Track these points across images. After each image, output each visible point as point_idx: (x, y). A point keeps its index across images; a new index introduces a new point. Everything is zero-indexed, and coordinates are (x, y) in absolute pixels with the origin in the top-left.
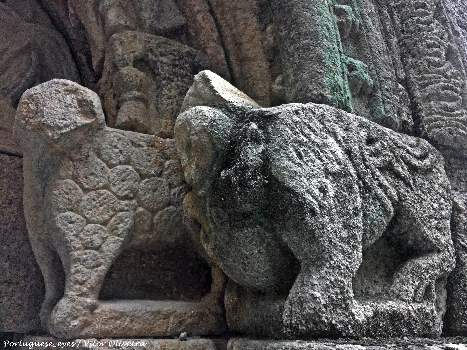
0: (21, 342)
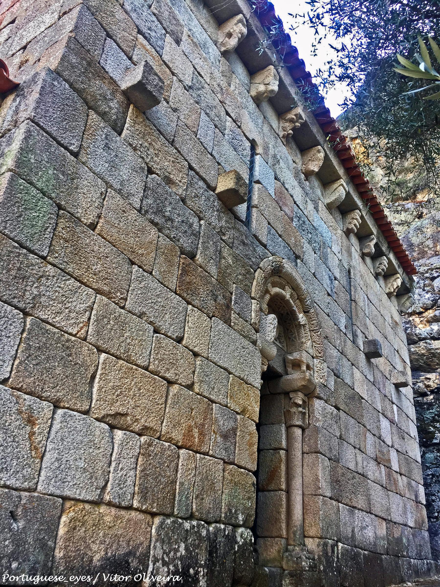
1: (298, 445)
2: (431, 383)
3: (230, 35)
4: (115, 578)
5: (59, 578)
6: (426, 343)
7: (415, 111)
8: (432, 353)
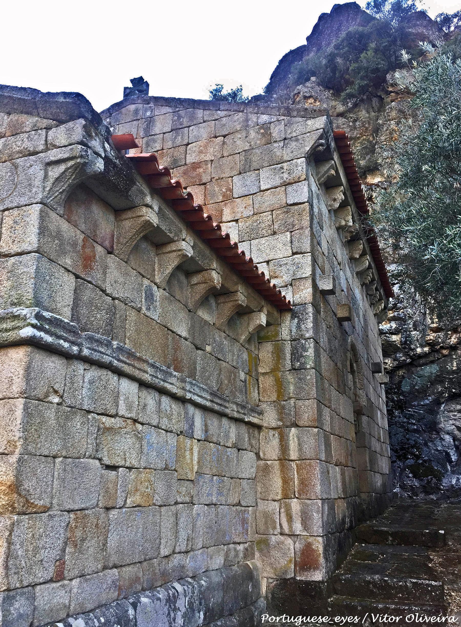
0: (284, 616)
3: (335, 200)
4: (385, 619)
5: (324, 619)
6: (386, 336)
8: (390, 344)
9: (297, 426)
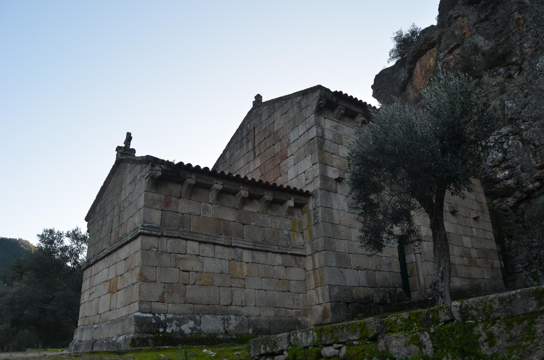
1: (419, 260)
2: (510, 204)
7: (260, 347)
9: (317, 252)
